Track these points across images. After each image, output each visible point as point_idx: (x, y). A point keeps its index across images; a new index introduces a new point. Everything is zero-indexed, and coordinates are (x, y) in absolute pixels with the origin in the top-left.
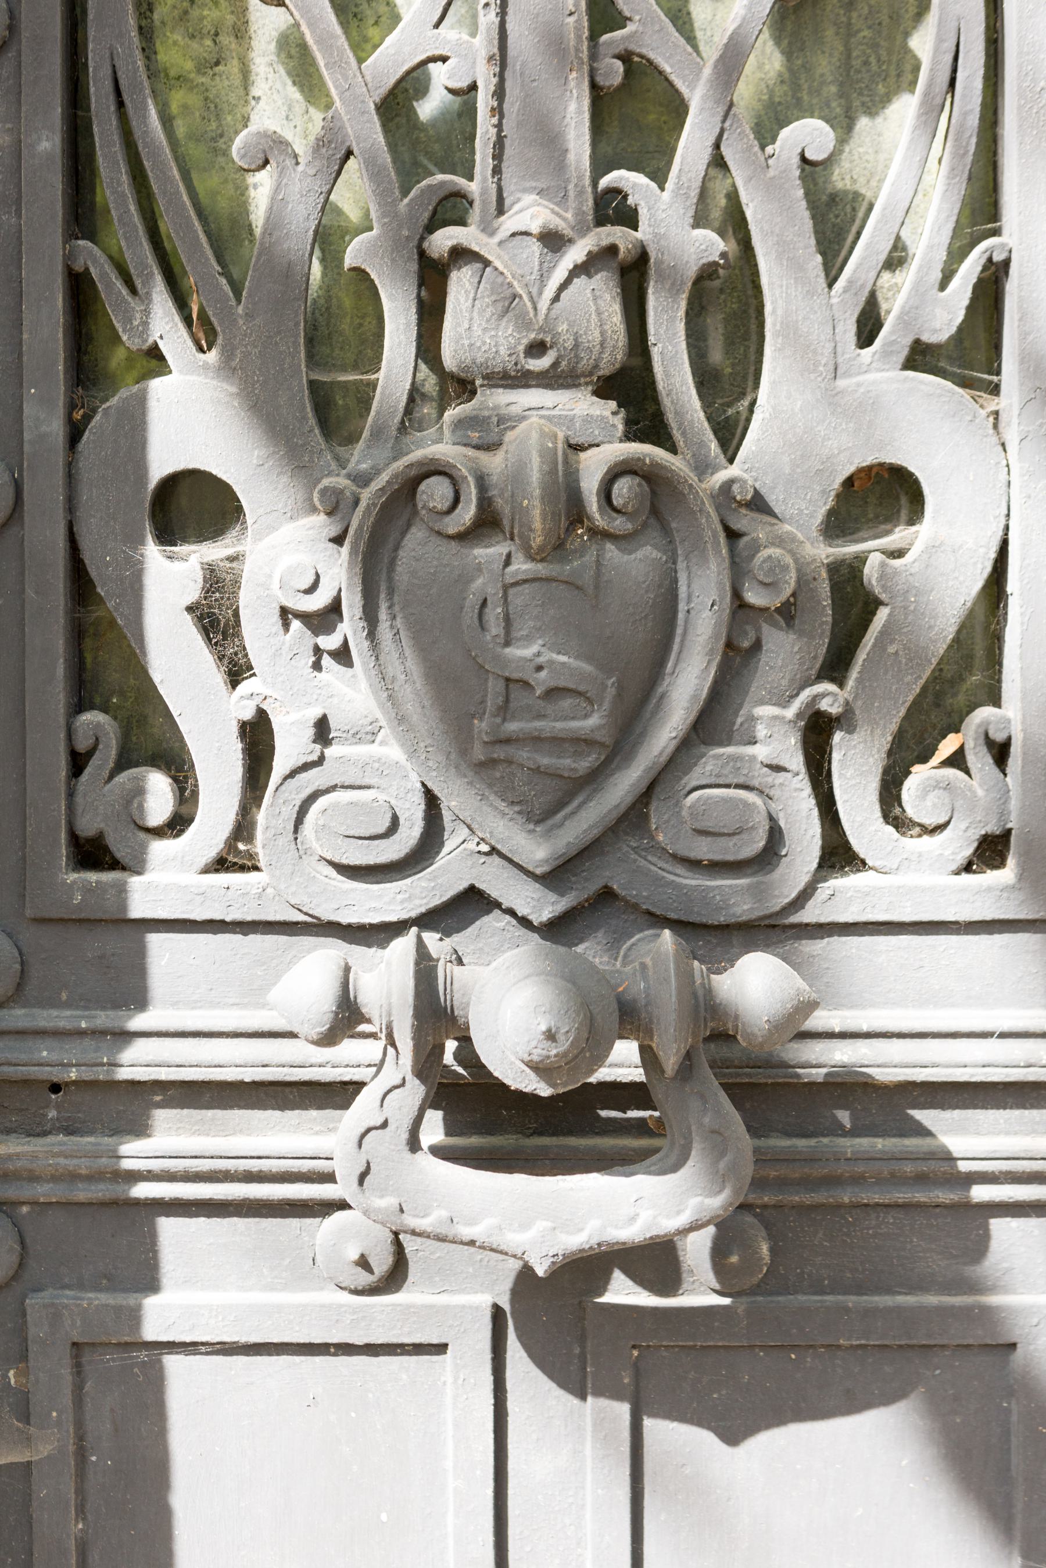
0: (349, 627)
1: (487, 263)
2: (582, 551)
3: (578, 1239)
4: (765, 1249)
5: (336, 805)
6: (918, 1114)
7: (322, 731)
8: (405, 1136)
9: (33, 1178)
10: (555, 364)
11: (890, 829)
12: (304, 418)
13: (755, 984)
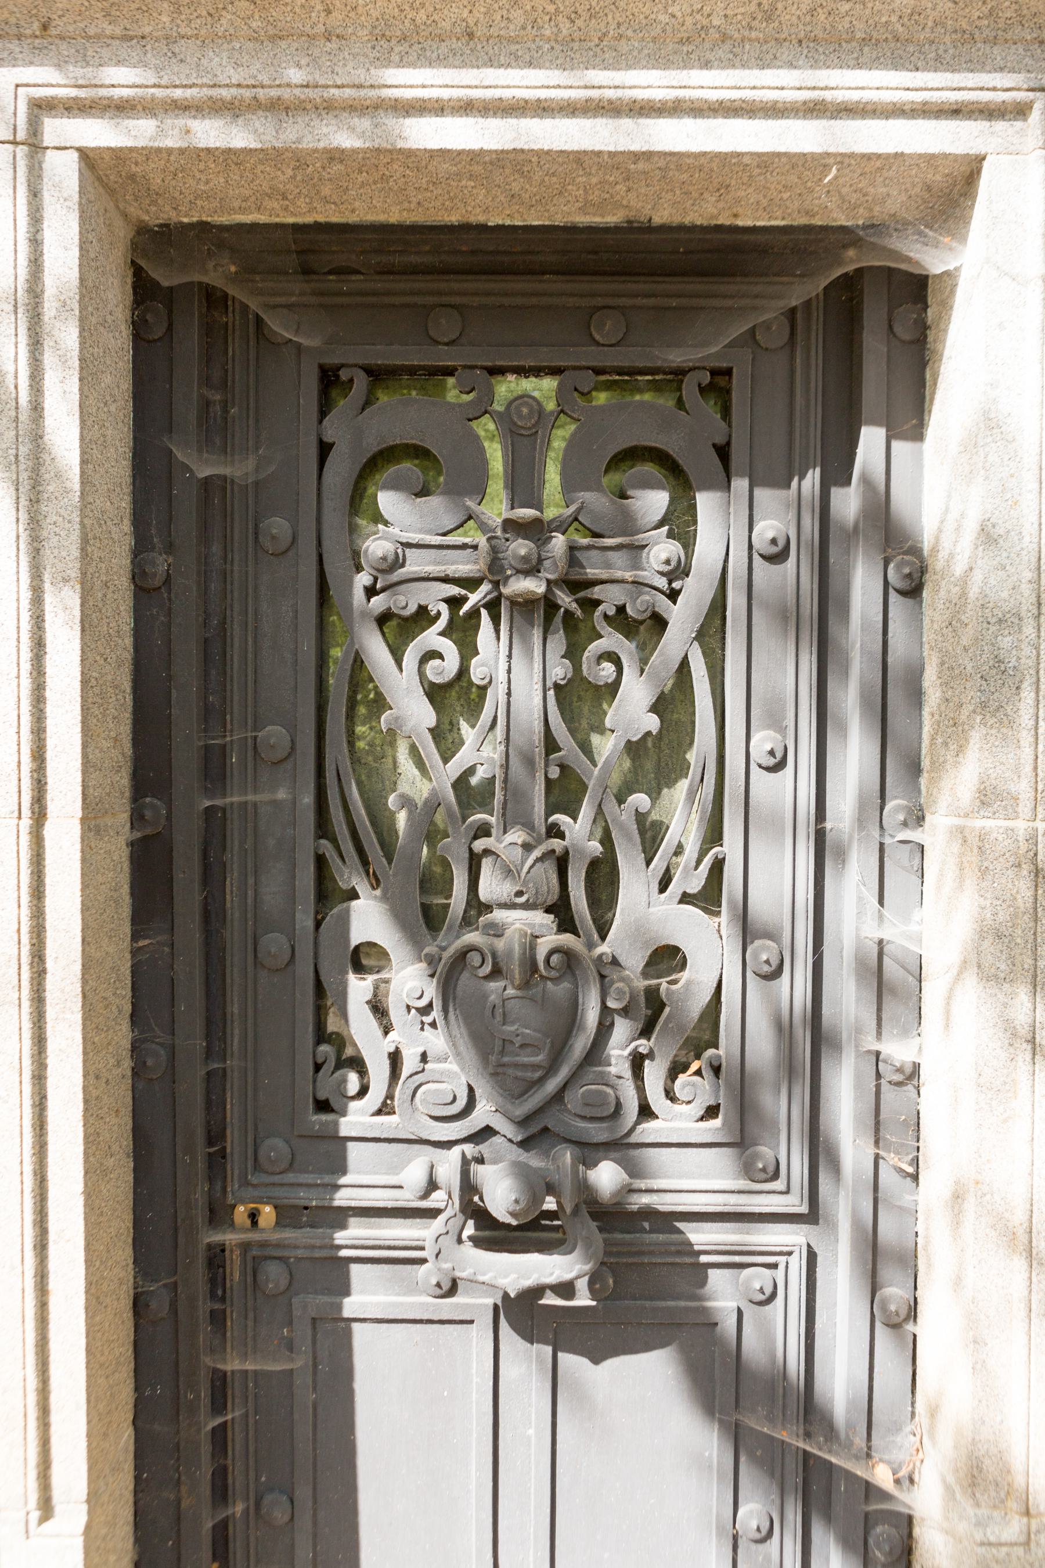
0: (436, 1014)
1: (498, 856)
2: (537, 985)
3: (528, 1282)
4: (611, 1281)
5: (429, 1091)
6: (678, 1225)
7: (424, 1057)
8: (456, 1238)
9: (296, 1247)
10: (528, 900)
11: (669, 1102)
12: (418, 920)
13: (606, 1176)
